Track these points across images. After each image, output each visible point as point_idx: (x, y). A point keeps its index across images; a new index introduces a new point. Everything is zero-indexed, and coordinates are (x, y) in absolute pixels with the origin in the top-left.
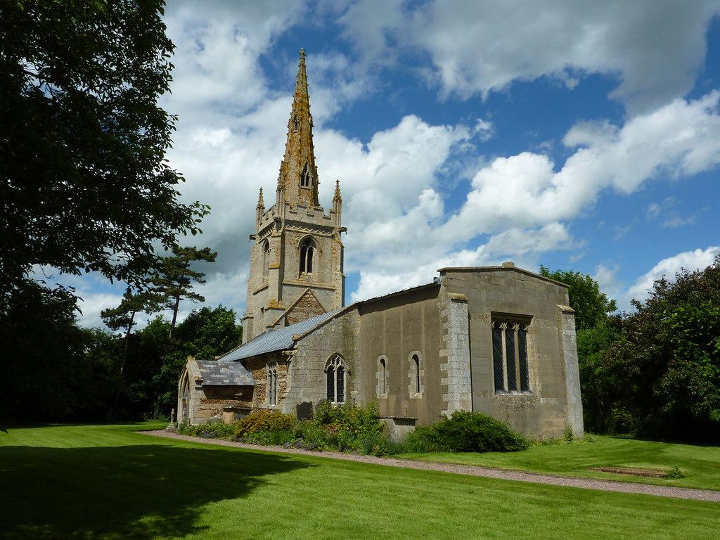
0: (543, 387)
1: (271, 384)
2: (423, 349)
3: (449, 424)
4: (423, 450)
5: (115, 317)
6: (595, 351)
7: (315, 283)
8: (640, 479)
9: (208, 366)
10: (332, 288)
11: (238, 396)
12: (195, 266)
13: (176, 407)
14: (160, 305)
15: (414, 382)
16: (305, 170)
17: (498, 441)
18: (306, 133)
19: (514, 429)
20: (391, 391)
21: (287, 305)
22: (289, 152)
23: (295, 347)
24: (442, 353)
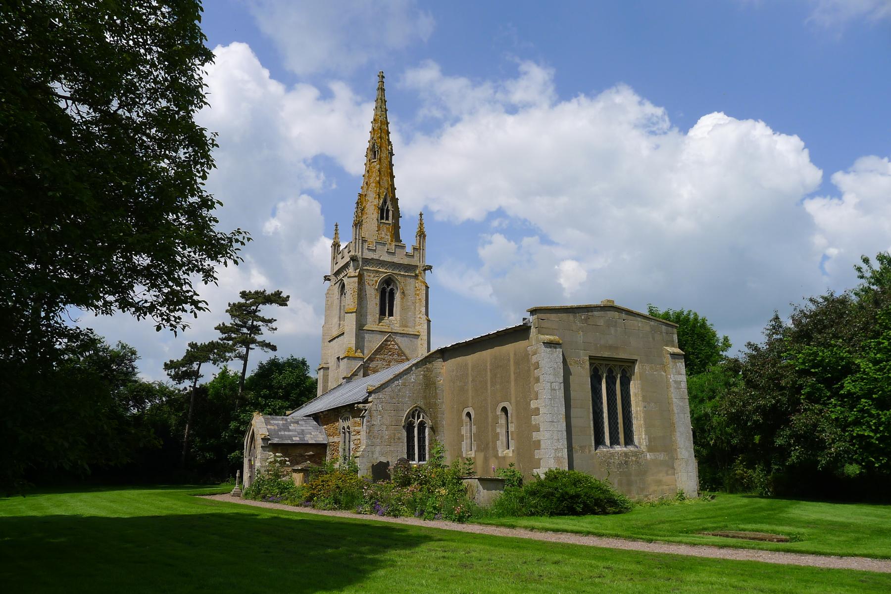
0: (650, 441)
1: (345, 442)
2: (513, 400)
3: (541, 484)
4: (514, 513)
5: (179, 369)
6: (710, 398)
7: (397, 328)
8: (753, 543)
9: (276, 422)
10: (418, 334)
11: (308, 455)
12: (266, 311)
13: (241, 467)
14: (228, 354)
15: (503, 438)
16: (385, 202)
17: (598, 503)
18: (385, 163)
19: (616, 490)
20: (478, 446)
21: (367, 354)
22: (367, 183)
23: (370, 399)
24: (533, 404)
